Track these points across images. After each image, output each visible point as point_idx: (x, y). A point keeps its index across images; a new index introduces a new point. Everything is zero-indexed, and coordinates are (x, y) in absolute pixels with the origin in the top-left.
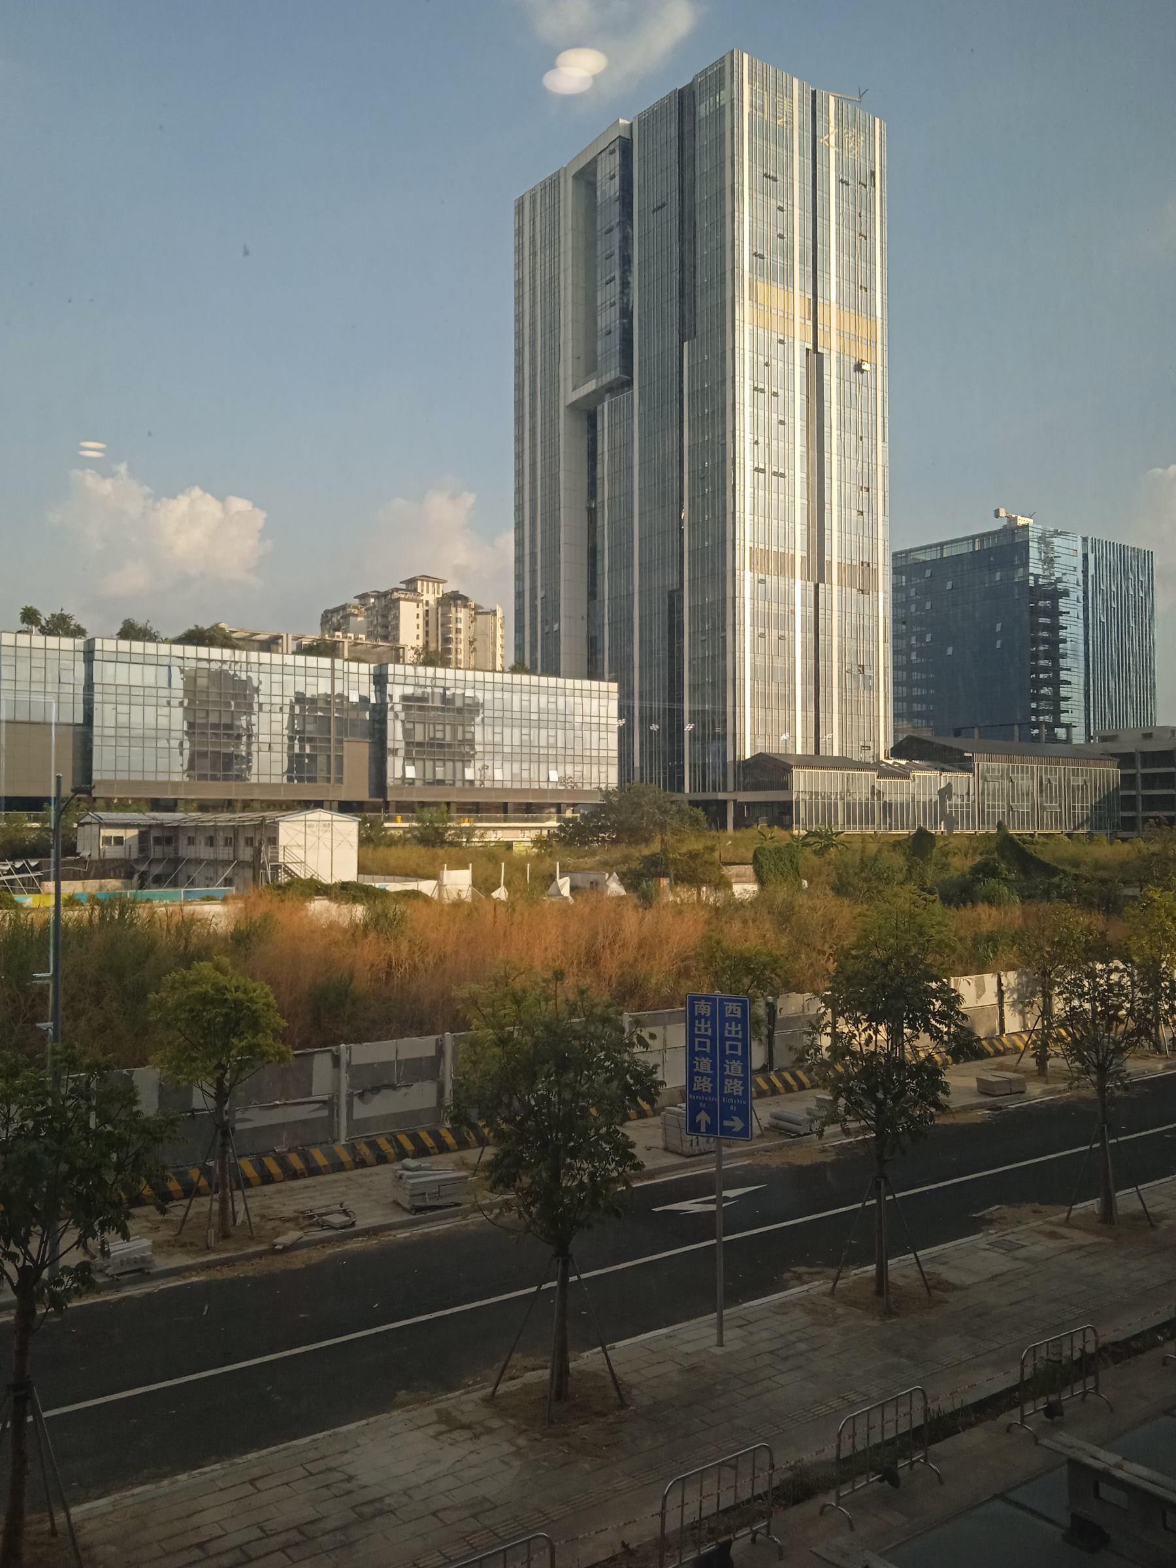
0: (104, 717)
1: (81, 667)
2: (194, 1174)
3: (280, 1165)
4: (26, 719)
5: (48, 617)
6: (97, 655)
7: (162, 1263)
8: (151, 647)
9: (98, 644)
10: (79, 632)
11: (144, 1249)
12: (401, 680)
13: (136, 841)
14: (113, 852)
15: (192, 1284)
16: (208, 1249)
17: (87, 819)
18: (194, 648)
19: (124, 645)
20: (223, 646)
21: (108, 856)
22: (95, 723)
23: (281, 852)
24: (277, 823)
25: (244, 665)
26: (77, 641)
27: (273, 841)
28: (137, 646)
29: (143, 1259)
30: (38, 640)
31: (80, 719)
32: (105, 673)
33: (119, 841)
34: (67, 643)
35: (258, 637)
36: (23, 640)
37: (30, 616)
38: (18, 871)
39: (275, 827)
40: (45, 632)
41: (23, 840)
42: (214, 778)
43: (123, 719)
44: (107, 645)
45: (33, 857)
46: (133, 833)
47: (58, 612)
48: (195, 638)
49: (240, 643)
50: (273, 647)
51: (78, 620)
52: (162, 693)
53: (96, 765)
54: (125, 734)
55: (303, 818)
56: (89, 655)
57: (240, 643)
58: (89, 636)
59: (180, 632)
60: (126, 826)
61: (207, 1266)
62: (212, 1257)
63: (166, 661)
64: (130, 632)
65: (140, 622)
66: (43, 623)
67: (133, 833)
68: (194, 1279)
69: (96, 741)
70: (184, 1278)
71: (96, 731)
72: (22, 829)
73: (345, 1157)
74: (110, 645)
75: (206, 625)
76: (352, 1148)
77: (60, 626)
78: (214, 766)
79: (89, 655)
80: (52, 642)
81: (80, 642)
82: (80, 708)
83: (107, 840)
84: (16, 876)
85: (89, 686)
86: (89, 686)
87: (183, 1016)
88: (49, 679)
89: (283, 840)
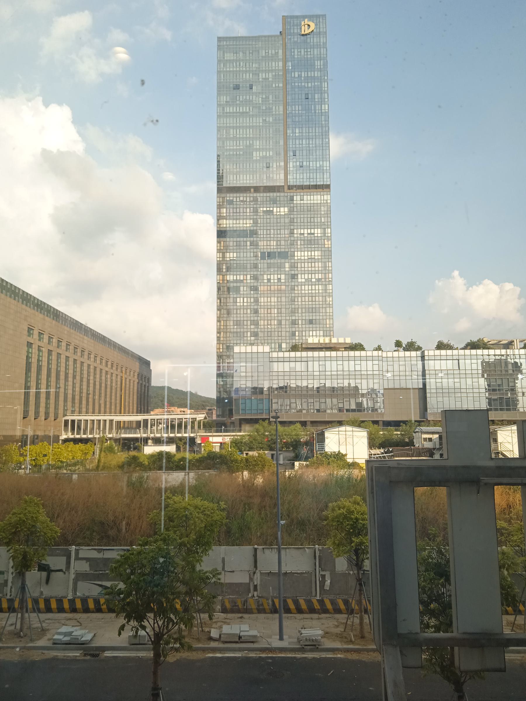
0: (431, 383)
1: (420, 363)
2: (302, 602)
3: (332, 604)
4: (399, 387)
5: (406, 343)
6: (426, 358)
7: (328, 644)
8: (449, 352)
9: (426, 353)
10: (419, 348)
11: (318, 635)
12: (439, 358)
13: (438, 440)
14: (428, 445)
15: (216, 657)
16: (351, 642)
17: (417, 430)
18: (475, 350)
19: (438, 352)
20: (484, 348)
21: (425, 446)
22: (427, 388)
23: (499, 446)
24: (324, 432)
25: (512, 356)
26: (418, 352)
27: (495, 440)
28: (443, 352)
29: (316, 640)
30: (402, 354)
31: (421, 386)
32: (430, 365)
33: (430, 440)
34: (414, 354)
35: (502, 342)
36: (396, 354)
37: (398, 344)
38: (386, 453)
39: (495, 433)
40: (405, 349)
41: (393, 439)
42: (501, 410)
43: (439, 385)
44: (430, 353)
45: (391, 447)
46: (437, 436)
47: (410, 341)
48: (473, 346)
49: (491, 346)
50: (510, 346)
51: (419, 343)
52: (456, 372)
53: (429, 406)
54: (442, 391)
55: (510, 429)
56: (423, 358)
57: (491, 346)
58: (423, 350)
59: (463, 345)
60: (433, 433)
61: (347, 651)
62: (351, 646)
63: (457, 357)
64: (441, 346)
65: (445, 342)
66: (404, 346)
67: (437, 436)
68: (339, 656)
69: (428, 395)
70: (222, 653)
71: (428, 391)
72: (393, 435)
73: (317, 606)
74: (431, 353)
75: (475, 339)
76: (321, 602)
77: (411, 346)
78: (501, 404)
79: (423, 358)
80: (408, 354)
81: (419, 353)
82: (421, 381)
83: (425, 439)
84: (385, 455)
85: (424, 371)
86: (424, 371)
87: (334, 524)
88: (407, 370)
89: (500, 439)
